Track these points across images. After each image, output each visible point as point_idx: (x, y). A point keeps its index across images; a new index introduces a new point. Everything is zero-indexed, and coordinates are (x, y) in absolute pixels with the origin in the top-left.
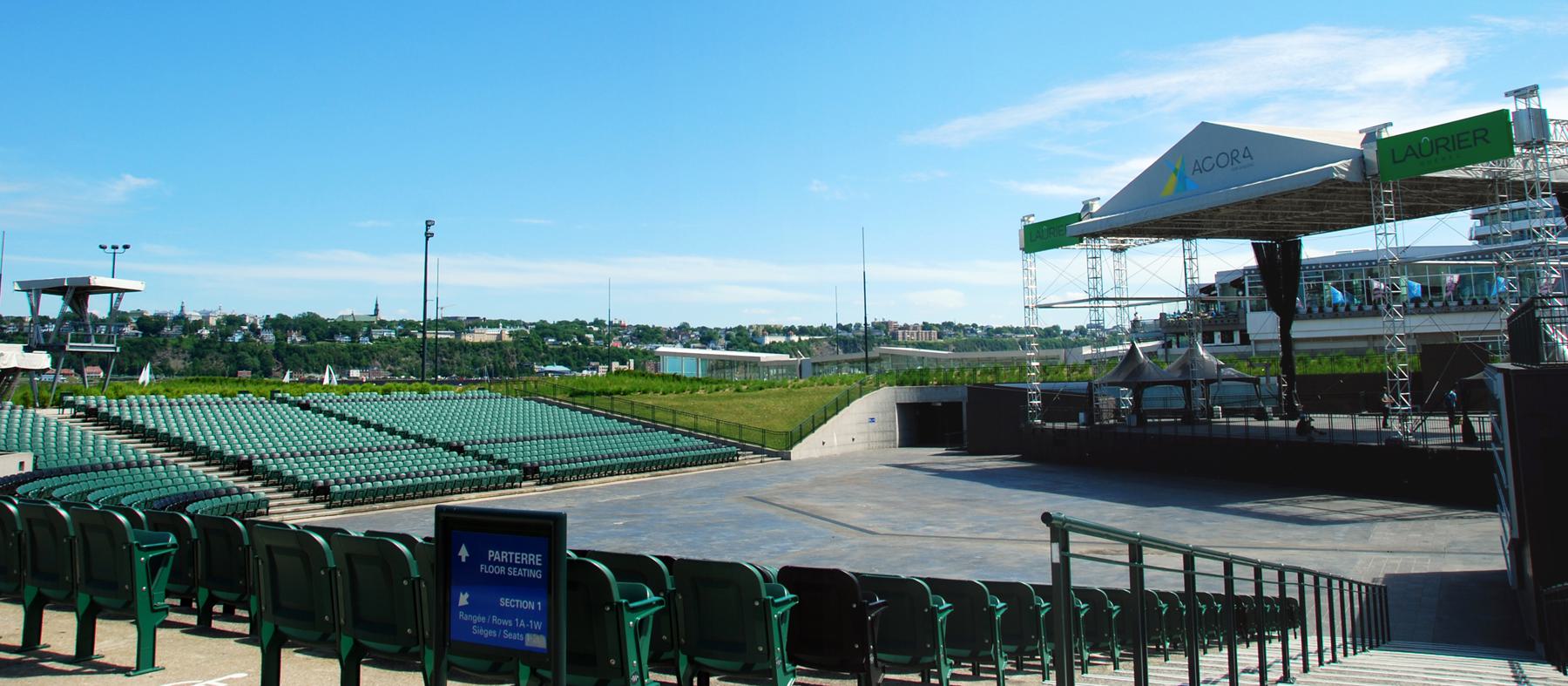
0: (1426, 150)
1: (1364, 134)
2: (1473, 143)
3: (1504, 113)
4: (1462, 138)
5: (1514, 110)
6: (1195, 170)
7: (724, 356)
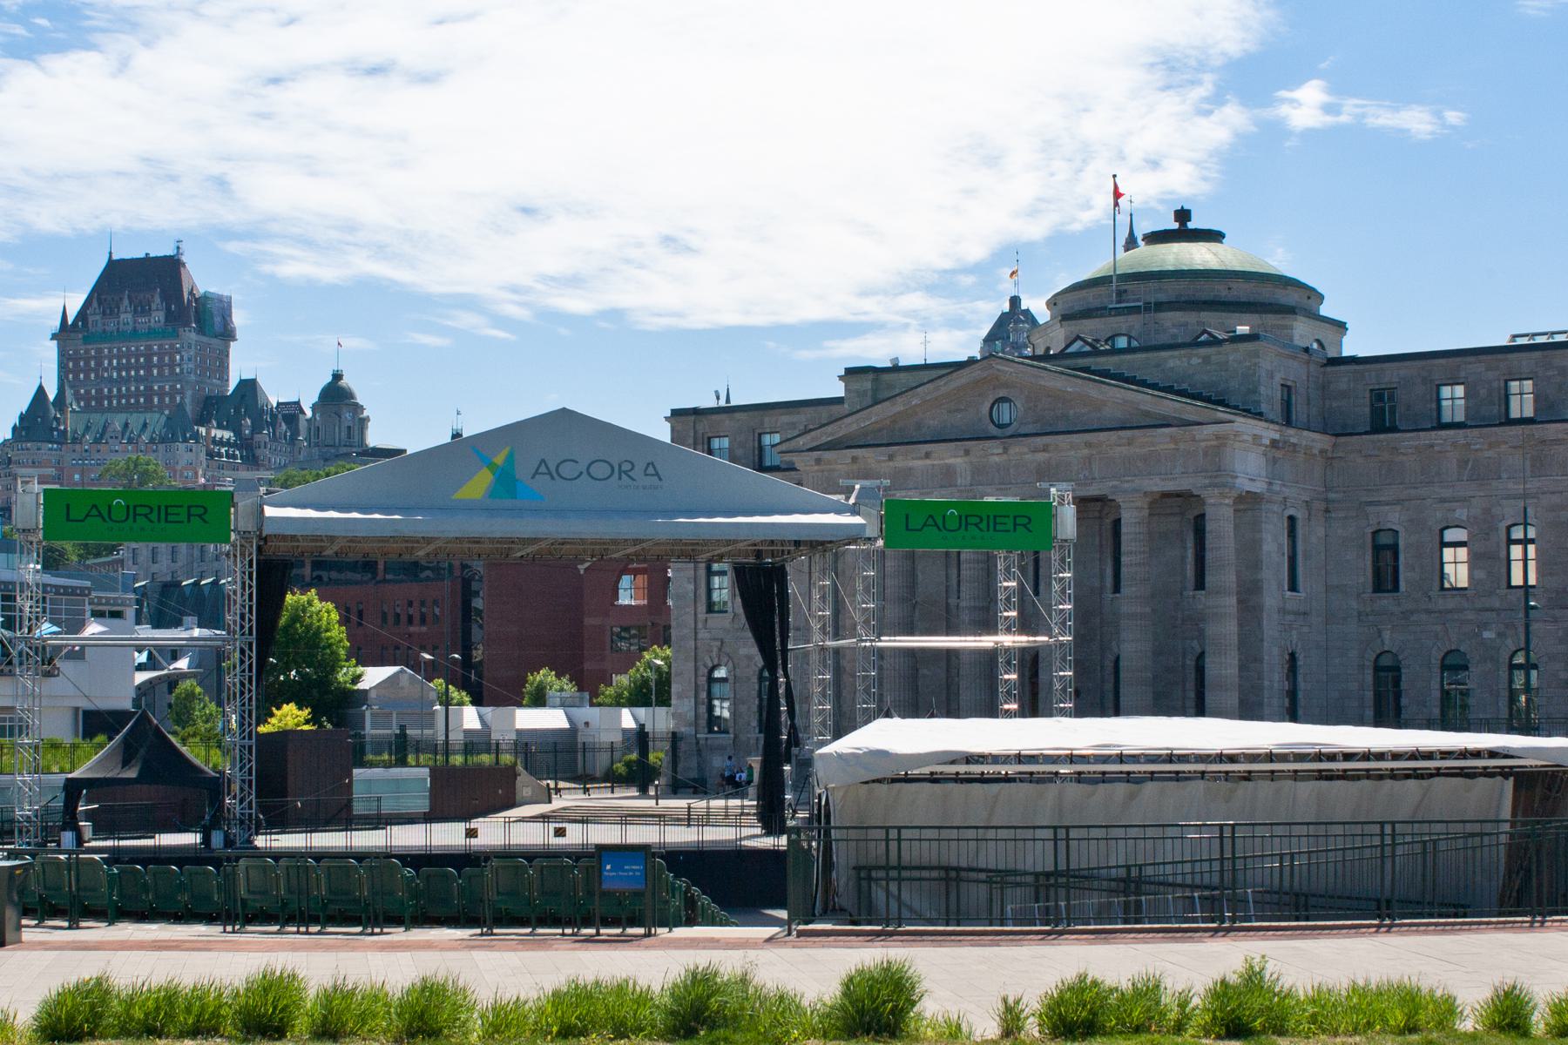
0: (119, 514)
2: (1012, 528)
6: (536, 472)
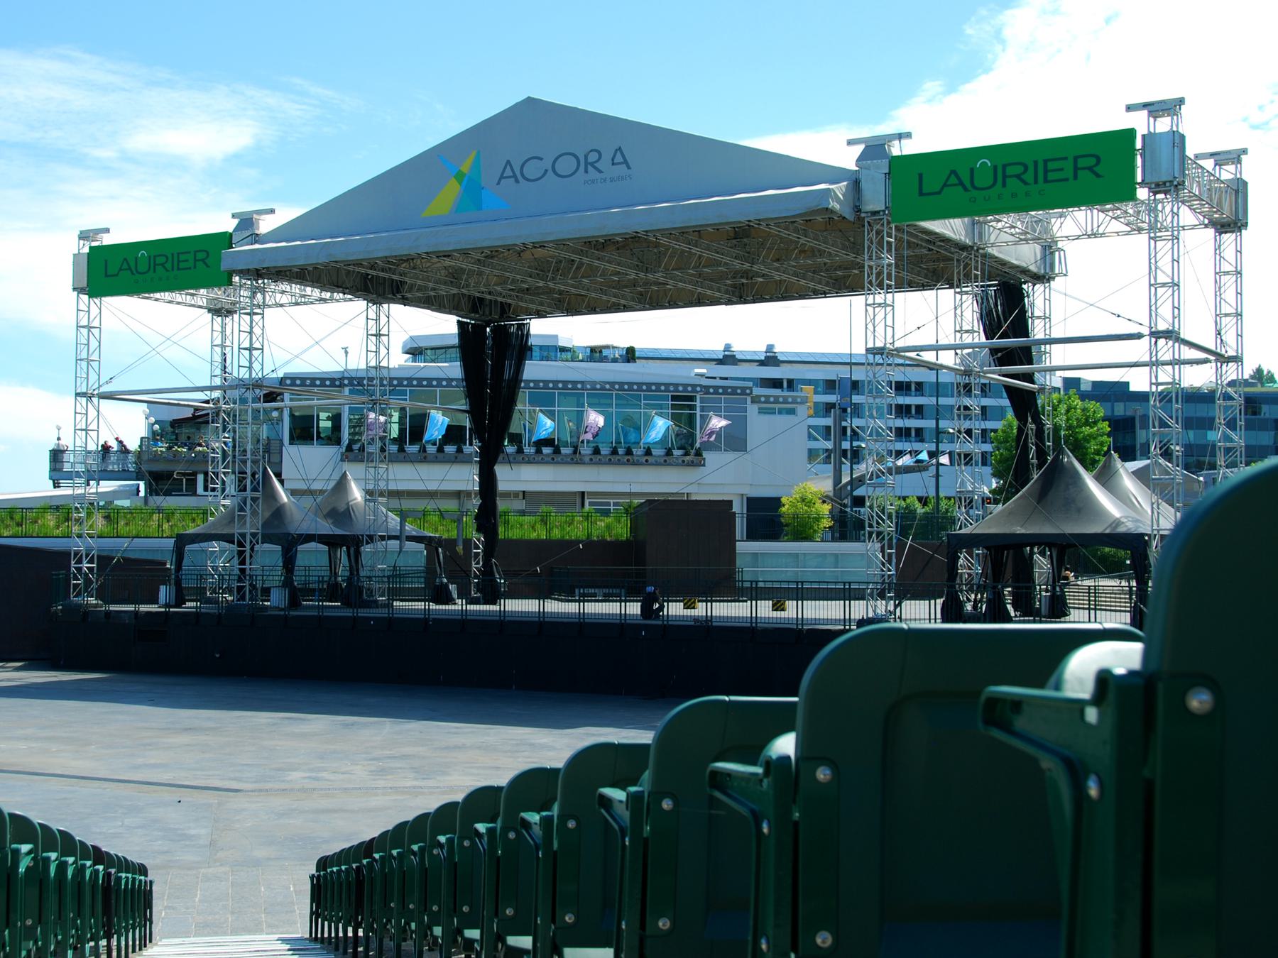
1: (861, 147)
2: (1070, 174)
3: (1130, 133)
4: (183, 257)
5: (1146, 132)
6: (502, 177)
7: (1018, 384)
